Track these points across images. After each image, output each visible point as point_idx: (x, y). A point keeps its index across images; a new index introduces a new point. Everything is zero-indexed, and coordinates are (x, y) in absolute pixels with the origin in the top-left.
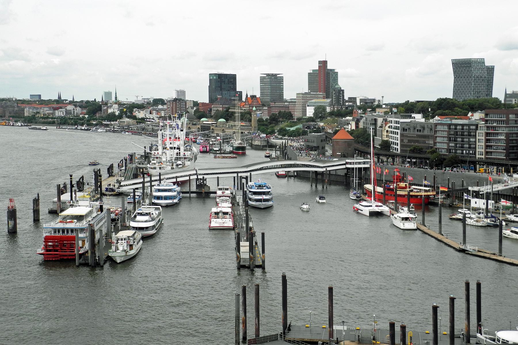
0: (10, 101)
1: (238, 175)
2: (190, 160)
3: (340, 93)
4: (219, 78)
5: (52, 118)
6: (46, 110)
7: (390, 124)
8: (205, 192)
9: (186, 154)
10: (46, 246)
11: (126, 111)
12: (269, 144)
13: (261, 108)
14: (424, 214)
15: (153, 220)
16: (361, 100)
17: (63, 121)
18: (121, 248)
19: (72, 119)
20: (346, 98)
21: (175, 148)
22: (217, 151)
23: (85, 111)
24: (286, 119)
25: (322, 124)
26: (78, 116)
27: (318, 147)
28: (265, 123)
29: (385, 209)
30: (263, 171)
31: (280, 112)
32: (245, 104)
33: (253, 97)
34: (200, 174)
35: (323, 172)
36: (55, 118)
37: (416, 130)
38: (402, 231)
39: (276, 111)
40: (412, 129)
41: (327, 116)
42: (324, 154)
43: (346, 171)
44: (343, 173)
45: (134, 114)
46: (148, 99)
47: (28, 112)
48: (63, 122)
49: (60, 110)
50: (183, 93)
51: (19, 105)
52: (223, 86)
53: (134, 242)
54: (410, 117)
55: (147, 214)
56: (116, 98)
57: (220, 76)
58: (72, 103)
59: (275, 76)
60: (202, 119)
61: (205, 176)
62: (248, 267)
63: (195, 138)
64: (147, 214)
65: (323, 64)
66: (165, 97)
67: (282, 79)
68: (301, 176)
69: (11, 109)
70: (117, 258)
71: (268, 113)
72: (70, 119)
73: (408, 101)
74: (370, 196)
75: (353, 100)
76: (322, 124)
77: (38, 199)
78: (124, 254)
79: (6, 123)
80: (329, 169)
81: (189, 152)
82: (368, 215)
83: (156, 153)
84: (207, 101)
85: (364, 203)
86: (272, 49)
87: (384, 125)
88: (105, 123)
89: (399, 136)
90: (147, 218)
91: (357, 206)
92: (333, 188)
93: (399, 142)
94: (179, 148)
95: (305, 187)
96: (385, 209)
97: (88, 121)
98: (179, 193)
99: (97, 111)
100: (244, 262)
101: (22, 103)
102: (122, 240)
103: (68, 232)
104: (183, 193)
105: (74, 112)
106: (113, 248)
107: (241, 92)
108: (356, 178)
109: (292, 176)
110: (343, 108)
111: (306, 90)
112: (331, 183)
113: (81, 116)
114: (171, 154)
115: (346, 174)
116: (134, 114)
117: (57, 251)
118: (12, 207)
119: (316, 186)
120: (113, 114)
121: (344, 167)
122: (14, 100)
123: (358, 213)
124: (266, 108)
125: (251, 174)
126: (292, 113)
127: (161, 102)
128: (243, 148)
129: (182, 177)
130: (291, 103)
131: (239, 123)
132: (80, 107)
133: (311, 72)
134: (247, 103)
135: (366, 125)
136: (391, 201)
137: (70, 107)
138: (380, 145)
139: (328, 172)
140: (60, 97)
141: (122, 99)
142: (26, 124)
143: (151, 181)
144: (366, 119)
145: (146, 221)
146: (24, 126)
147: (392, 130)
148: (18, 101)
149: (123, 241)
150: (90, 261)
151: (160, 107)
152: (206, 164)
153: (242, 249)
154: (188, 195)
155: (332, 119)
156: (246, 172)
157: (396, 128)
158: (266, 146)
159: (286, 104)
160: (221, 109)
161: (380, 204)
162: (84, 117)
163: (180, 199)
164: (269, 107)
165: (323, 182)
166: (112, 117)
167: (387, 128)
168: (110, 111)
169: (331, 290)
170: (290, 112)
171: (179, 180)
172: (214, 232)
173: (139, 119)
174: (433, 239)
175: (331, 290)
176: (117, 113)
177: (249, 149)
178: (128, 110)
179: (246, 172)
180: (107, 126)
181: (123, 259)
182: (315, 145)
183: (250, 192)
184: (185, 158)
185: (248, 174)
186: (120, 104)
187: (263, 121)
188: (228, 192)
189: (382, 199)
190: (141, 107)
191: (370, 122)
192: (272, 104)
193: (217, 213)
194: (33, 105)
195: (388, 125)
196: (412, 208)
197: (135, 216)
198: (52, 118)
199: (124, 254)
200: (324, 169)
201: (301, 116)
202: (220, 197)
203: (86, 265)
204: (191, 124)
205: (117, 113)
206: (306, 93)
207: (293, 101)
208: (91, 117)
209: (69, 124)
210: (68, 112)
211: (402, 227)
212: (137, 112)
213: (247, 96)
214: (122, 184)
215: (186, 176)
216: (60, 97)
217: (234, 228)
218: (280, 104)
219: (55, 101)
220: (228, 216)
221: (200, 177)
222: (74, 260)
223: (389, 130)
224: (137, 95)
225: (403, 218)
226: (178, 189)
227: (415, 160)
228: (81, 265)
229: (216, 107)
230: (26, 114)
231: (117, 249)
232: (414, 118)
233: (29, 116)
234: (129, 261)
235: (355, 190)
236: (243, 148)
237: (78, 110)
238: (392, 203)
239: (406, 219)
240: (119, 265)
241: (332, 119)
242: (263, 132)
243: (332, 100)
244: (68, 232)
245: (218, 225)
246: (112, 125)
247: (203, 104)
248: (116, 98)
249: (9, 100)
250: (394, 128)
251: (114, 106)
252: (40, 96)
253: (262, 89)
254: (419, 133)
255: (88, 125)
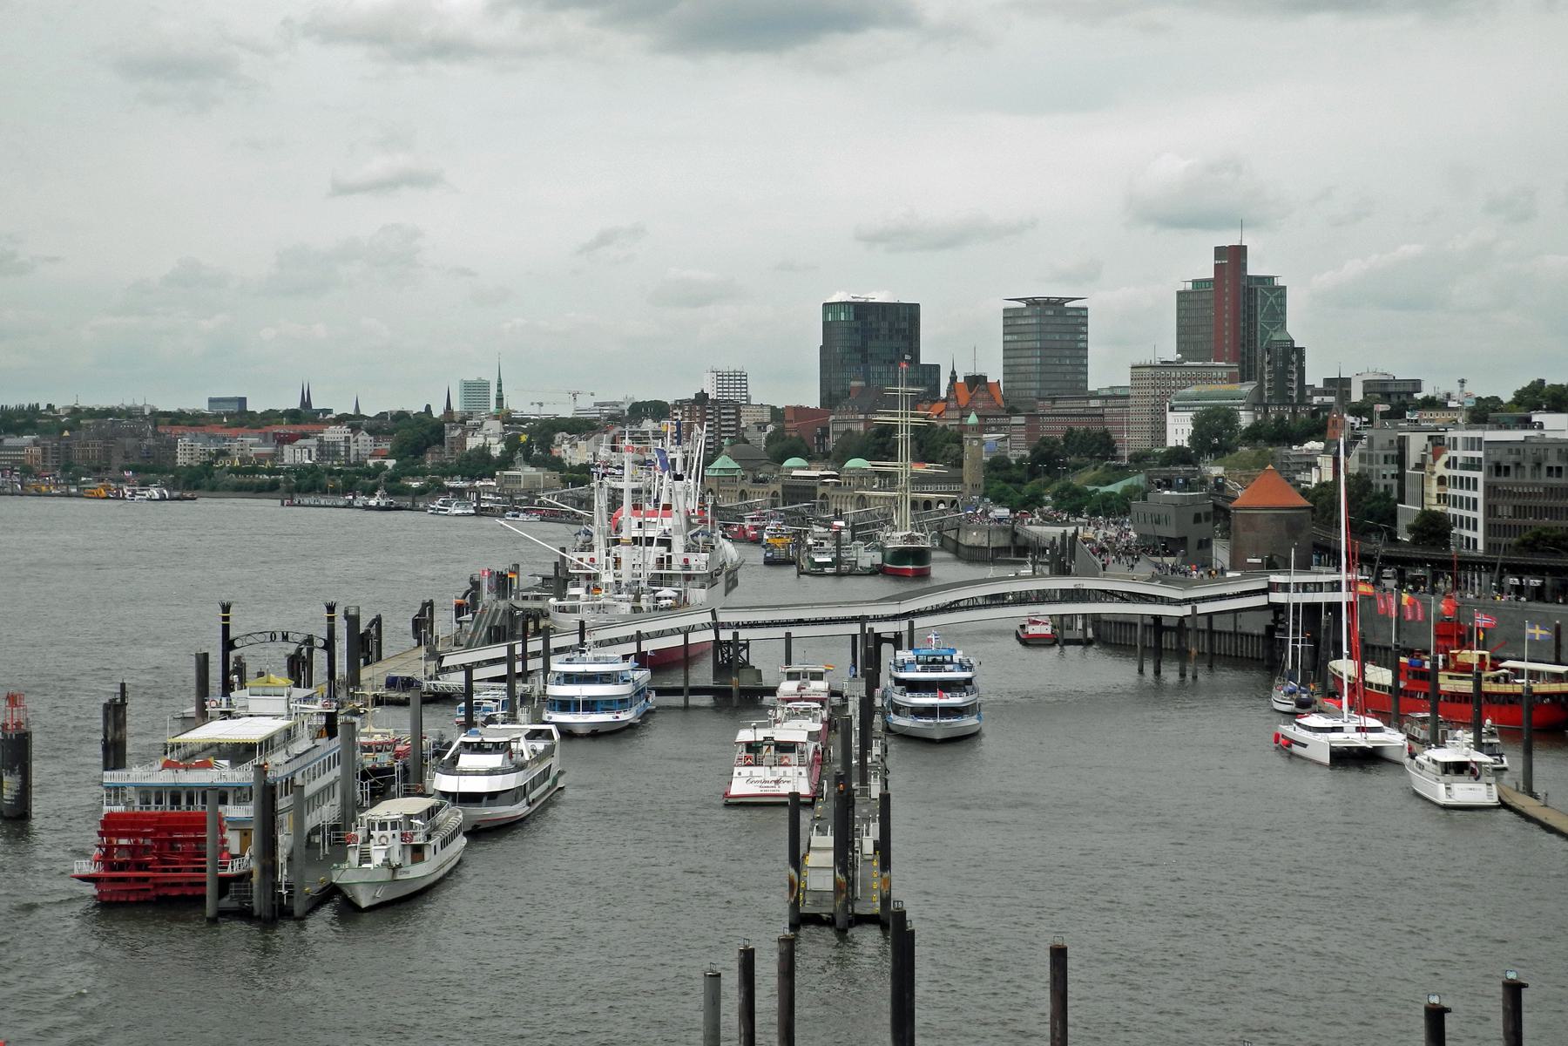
0: (130, 417)
1: (863, 628)
2: (711, 579)
3: (1288, 361)
4: (857, 317)
5: (270, 472)
6: (251, 445)
7: (1452, 453)
8: (743, 691)
9: (692, 562)
10: (108, 850)
11: (529, 442)
12: (1020, 542)
13: (1004, 420)
14: (1528, 752)
15: (519, 767)
16: (1367, 384)
17: (306, 482)
18: (378, 858)
19: (340, 472)
20: (1314, 378)
21: (650, 541)
22: (826, 564)
23: (386, 446)
24: (1092, 456)
25: (1217, 471)
26: (360, 463)
27: (1183, 541)
28: (1015, 472)
29: (1392, 739)
30: (977, 629)
31: (1070, 433)
32: (947, 409)
33: (976, 381)
34: (728, 626)
35: (1182, 619)
36: (278, 472)
37: (1544, 471)
38: (1441, 812)
39: (1055, 430)
40: (1528, 466)
41: (1238, 444)
42: (1206, 564)
43: (1268, 618)
44: (1256, 625)
45: (556, 452)
46: (615, 404)
47: (188, 451)
48: (305, 485)
49: (301, 442)
50: (740, 378)
51: (161, 430)
52: (874, 346)
53: (429, 837)
54: (1526, 423)
55: (497, 748)
56: (500, 400)
57: (862, 311)
58: (354, 422)
59: (1057, 304)
60: (789, 463)
61: (744, 634)
62: (830, 922)
63: (756, 528)
64: (497, 748)
65: (1232, 257)
66: (668, 396)
67: (1082, 314)
68: (1109, 636)
69: (130, 442)
70: (359, 888)
71: (1029, 437)
72: (330, 472)
73: (1542, 382)
74: (1335, 695)
75: (1338, 385)
76: (1217, 471)
77: (124, 704)
78: (385, 875)
79: (108, 489)
80: (1203, 608)
81: (705, 556)
82: (1327, 760)
83: (586, 560)
84: (813, 401)
85: (1315, 720)
86: (1017, 184)
87: (1430, 457)
88: (452, 484)
89: (1479, 495)
90: (495, 760)
91: (1289, 730)
92: (1227, 677)
93: (1479, 515)
94: (666, 542)
95: (1117, 672)
96: (1392, 739)
97: (394, 477)
98: (640, 693)
99: (429, 445)
100: (815, 903)
101: (172, 423)
102: (383, 826)
103: (190, 801)
104: (661, 692)
105: (348, 449)
106: (354, 857)
107: (936, 368)
108: (1295, 632)
109: (1077, 642)
110: (1295, 415)
111: (1172, 354)
112: (1213, 659)
113: (371, 462)
114: (640, 562)
115: (1270, 630)
116: (556, 452)
117: (140, 866)
118: (18, 724)
119: (1157, 672)
120: (483, 451)
121: (1261, 601)
122: (147, 412)
123: (1292, 754)
124: (1020, 420)
125: (911, 624)
126: (1114, 436)
127: (659, 410)
128: (920, 556)
129: (661, 634)
130: (1111, 402)
131: (905, 466)
132: (370, 432)
133: (1189, 286)
134: (952, 405)
135: (1371, 462)
136: (1420, 715)
137: (334, 434)
138: (1411, 529)
139: (1203, 624)
140: (306, 403)
141: (519, 404)
142: (176, 494)
143: (546, 654)
144: (1371, 439)
145: (491, 772)
146: (172, 499)
147: (1458, 473)
148: (157, 416)
149: (389, 833)
150: (258, 903)
151: (648, 425)
152: (766, 594)
153: (812, 860)
154: (678, 701)
155: (1254, 453)
156: (896, 617)
157: (1472, 465)
158: (1006, 550)
159: (1093, 403)
160: (861, 427)
161: (1373, 722)
162: (380, 468)
163: (647, 715)
164: (1033, 416)
165: (1182, 655)
166: (480, 465)
167: (1440, 469)
168: (473, 442)
169: (1059, 956)
170: (1106, 434)
171: (648, 646)
172: (743, 815)
173: (572, 469)
174: (1554, 837)
175: (1059, 956)
176: (497, 450)
177: (941, 560)
178: (536, 439)
179: (896, 617)
180: (460, 493)
181: (381, 895)
182: (1170, 532)
183: (899, 682)
184: (688, 578)
185: (903, 626)
186: (507, 419)
187: (1009, 466)
188: (820, 686)
189: (1388, 707)
190: (580, 427)
191: (1382, 454)
192: (1044, 407)
193: (752, 747)
194: (208, 430)
195: (1444, 458)
196: (1492, 734)
197: (455, 759)
198: (270, 472)
199: (385, 875)
200: (1186, 610)
201: (1145, 445)
202: (789, 701)
203: (245, 914)
204: (749, 480)
205: (497, 450)
206: (1166, 365)
207: (1119, 392)
208: (407, 465)
209: (325, 492)
210: (326, 450)
211: (1442, 799)
212: (566, 446)
213: (953, 378)
214: (446, 663)
215: (673, 632)
216: (306, 403)
217: (814, 799)
218: (1069, 404)
219: (293, 416)
220: (793, 757)
221: (726, 635)
222: (200, 900)
223: (1448, 473)
224: (574, 390)
225: (1449, 770)
226: (643, 675)
227: (1538, 582)
228: (223, 913)
229: (844, 422)
230: (182, 459)
231: (365, 857)
232: (1541, 426)
233: (190, 466)
234: (406, 902)
235: (1292, 678)
236: (920, 556)
237: (364, 441)
238: (1424, 720)
239: (1459, 768)
240: (367, 919)
241: (1254, 453)
242: (999, 501)
243: (1261, 386)
244: (190, 801)
245: (757, 791)
246: (473, 489)
247: (799, 411)
248: (500, 400)
249: (129, 413)
250: (1465, 467)
251: (489, 424)
252: (243, 401)
253: (1009, 353)
254: (1554, 480)
255: (391, 493)
